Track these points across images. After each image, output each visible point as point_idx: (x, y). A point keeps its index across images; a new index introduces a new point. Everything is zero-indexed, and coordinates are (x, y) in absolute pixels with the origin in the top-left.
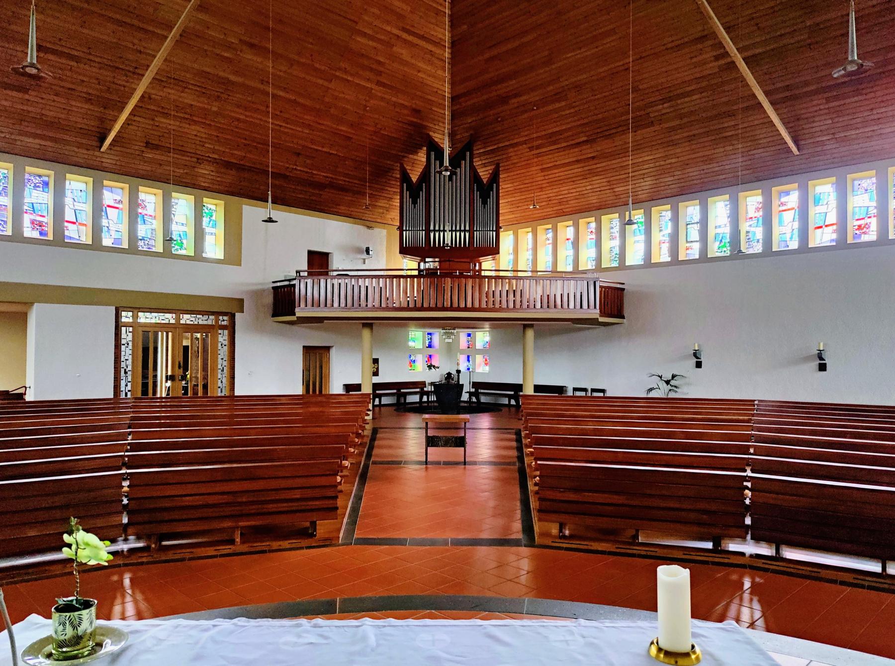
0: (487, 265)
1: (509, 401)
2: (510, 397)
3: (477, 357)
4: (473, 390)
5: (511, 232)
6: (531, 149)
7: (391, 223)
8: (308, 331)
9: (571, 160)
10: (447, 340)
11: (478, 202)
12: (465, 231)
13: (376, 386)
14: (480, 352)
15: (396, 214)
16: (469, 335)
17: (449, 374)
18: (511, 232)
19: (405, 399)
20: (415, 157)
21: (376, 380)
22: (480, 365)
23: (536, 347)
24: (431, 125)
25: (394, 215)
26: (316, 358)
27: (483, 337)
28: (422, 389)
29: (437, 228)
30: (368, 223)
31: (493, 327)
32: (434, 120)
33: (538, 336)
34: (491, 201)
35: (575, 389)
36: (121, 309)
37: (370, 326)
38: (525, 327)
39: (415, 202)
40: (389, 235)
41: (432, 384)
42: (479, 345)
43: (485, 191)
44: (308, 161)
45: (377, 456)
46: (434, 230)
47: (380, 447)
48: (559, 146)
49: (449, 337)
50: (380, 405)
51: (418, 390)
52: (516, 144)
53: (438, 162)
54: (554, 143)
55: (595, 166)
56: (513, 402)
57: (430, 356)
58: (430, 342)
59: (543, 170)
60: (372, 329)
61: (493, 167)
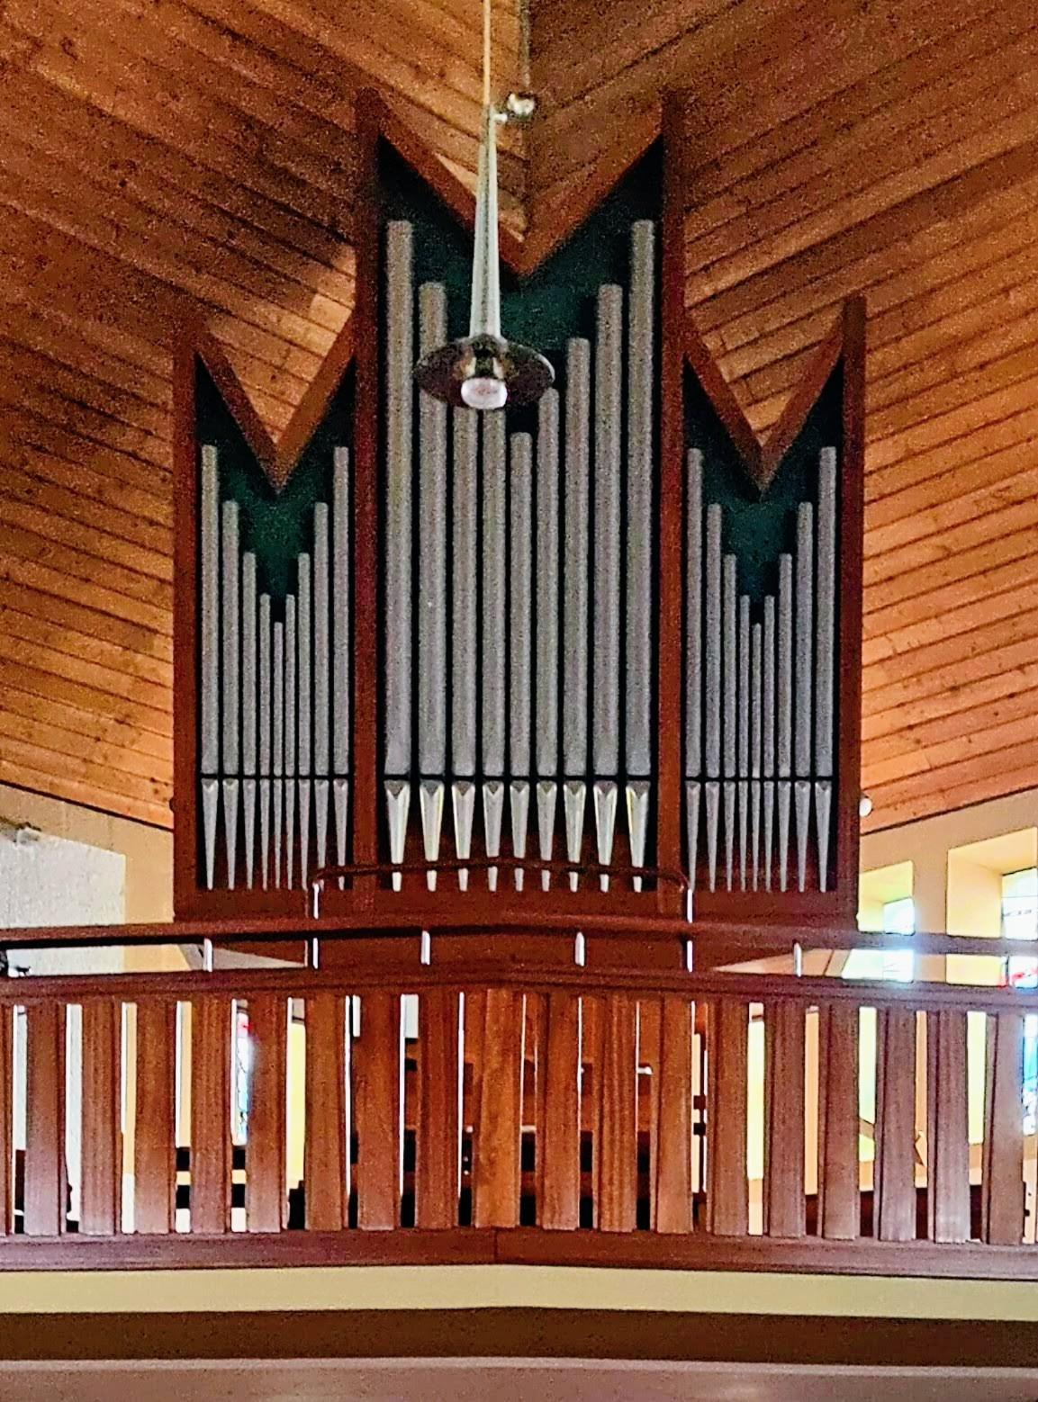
11: (715, 572)
12: (622, 778)
39: (278, 582)
43: (763, 486)
46: (703, 778)
53: (435, 294)
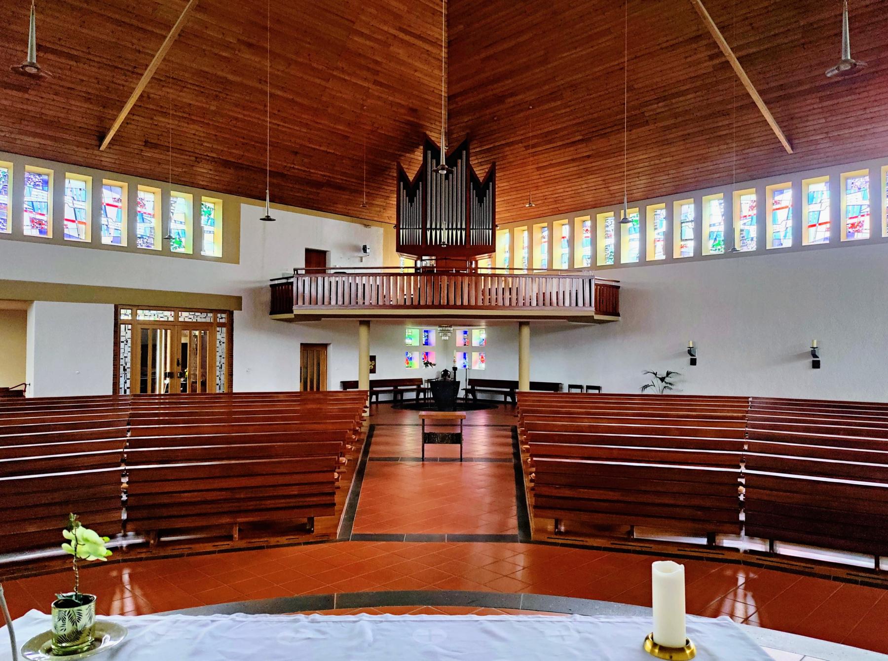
0: (483, 263)
1: (505, 398)
2: (506, 394)
3: (473, 355)
4: (470, 387)
5: (507, 230)
6: (527, 148)
7: (388, 221)
8: (305, 328)
9: (567, 159)
10: (443, 338)
11: (474, 200)
12: (461, 229)
13: (373, 383)
14: (476, 349)
15: (393, 212)
16: (465, 333)
17: (446, 371)
18: (507, 230)
19: (402, 396)
20: (412, 156)
21: (373, 377)
22: (476, 362)
23: (532, 345)
24: (428, 124)
25: (391, 214)
26: (313, 356)
27: (479, 335)
28: (419, 386)
29: (434, 226)
30: (365, 222)
31: (489, 325)
32: (430, 119)
33: (533, 333)
34: (487, 200)
35: (571, 386)
36: (120, 307)
37: (367, 324)
38: (521, 324)
39: (411, 201)
40: (386, 233)
41: (429, 381)
42: (475, 342)
43: (482, 190)
44: (306, 160)
45: (374, 452)
47: (377, 444)
48: (555, 145)
49: (445, 335)
50: (377, 402)
51: (415, 387)
52: (512, 143)
53: (434, 161)
54: (550, 142)
55: (590, 165)
56: (509, 399)
57: (427, 354)
58: (427, 340)
59: (538, 169)
60: (369, 326)
61: (489, 166)
